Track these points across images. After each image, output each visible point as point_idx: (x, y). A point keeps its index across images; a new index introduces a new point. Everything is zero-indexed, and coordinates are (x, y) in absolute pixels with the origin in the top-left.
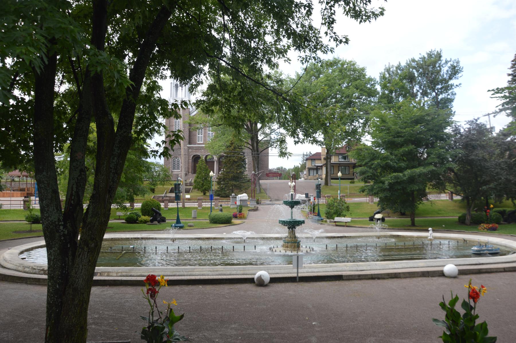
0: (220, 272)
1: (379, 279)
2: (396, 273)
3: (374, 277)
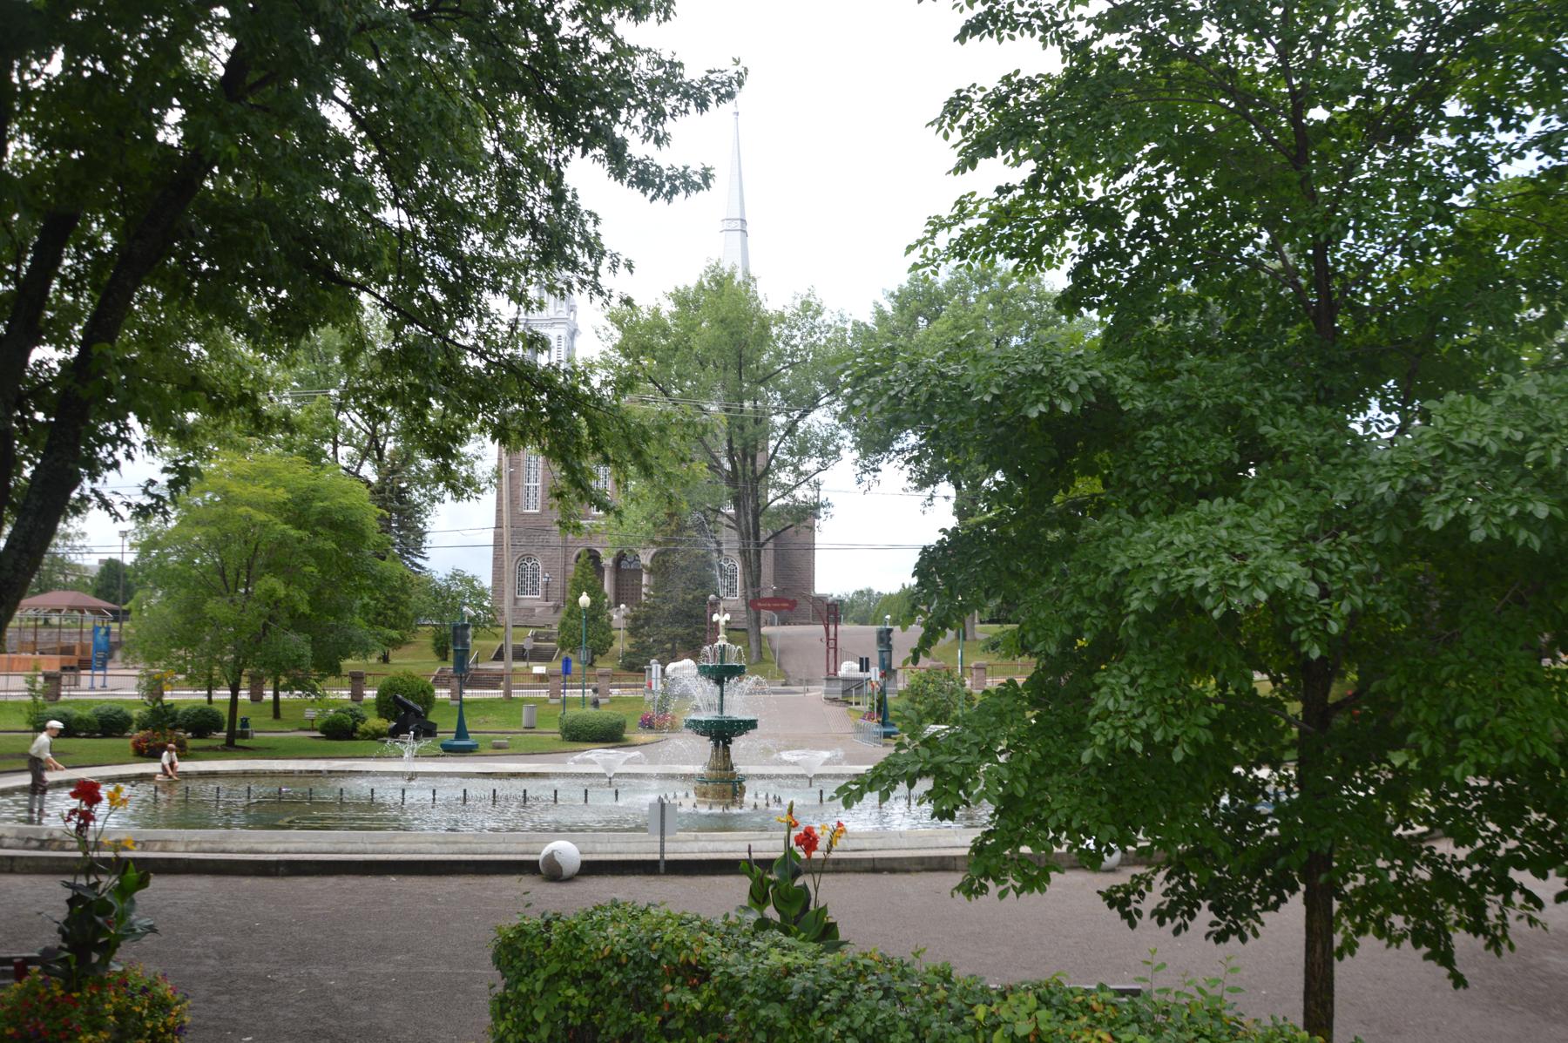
0: (462, 847)
1: (892, 871)
2: (943, 858)
3: (878, 866)
